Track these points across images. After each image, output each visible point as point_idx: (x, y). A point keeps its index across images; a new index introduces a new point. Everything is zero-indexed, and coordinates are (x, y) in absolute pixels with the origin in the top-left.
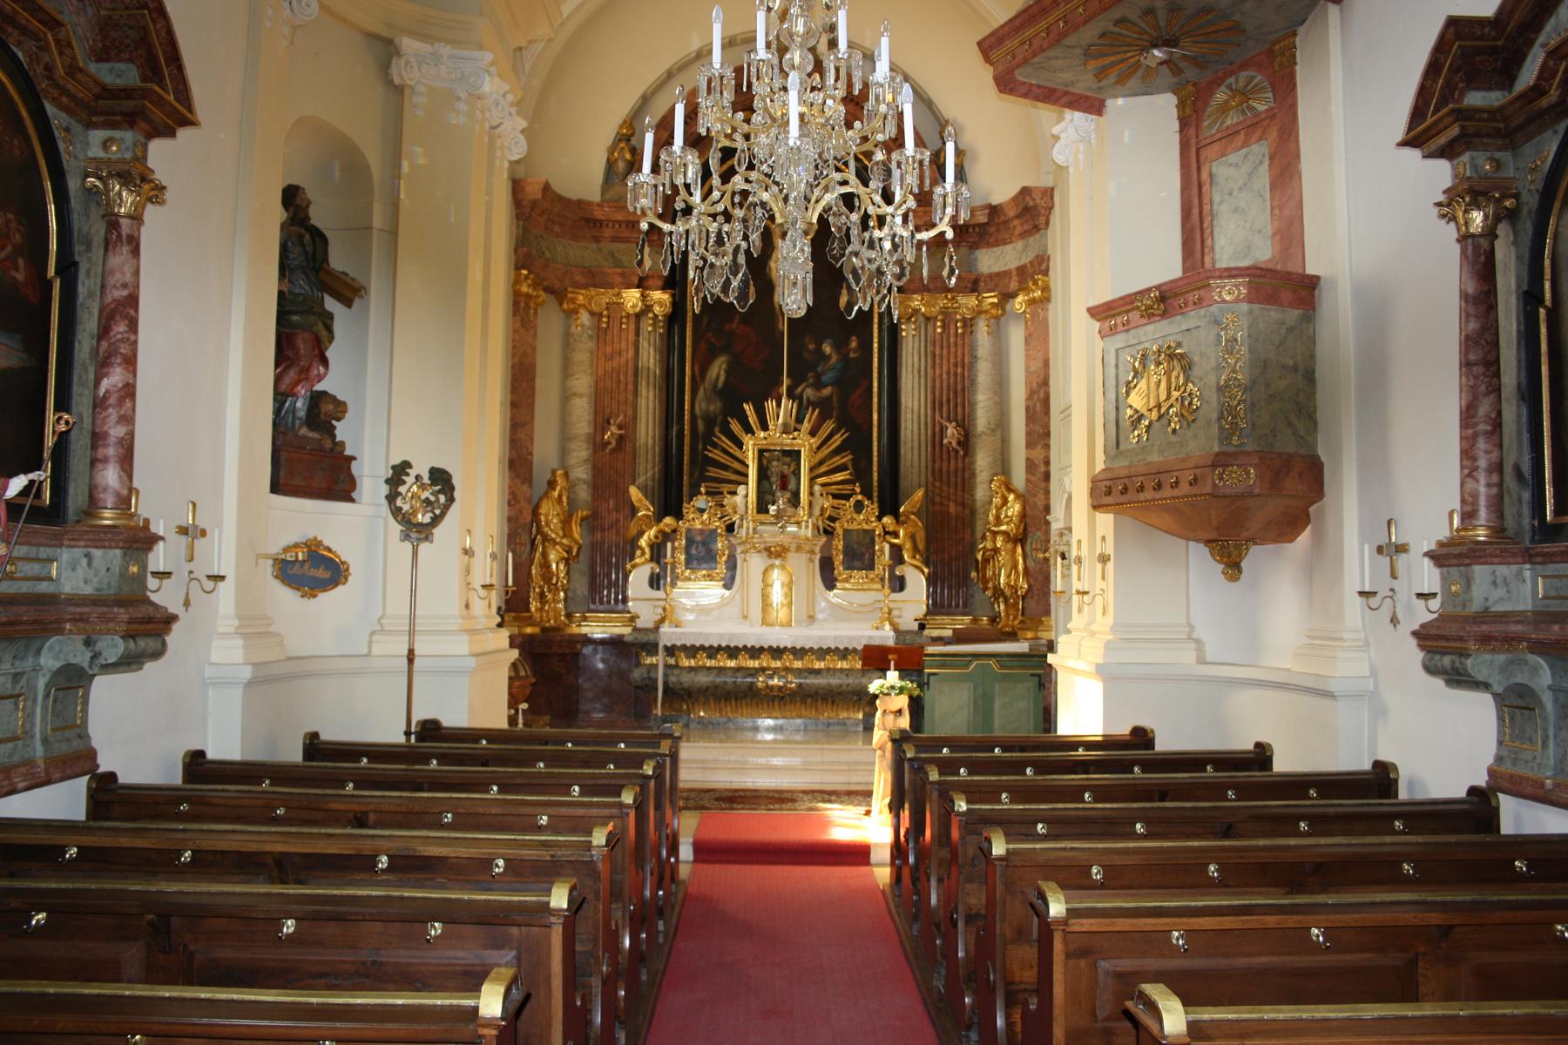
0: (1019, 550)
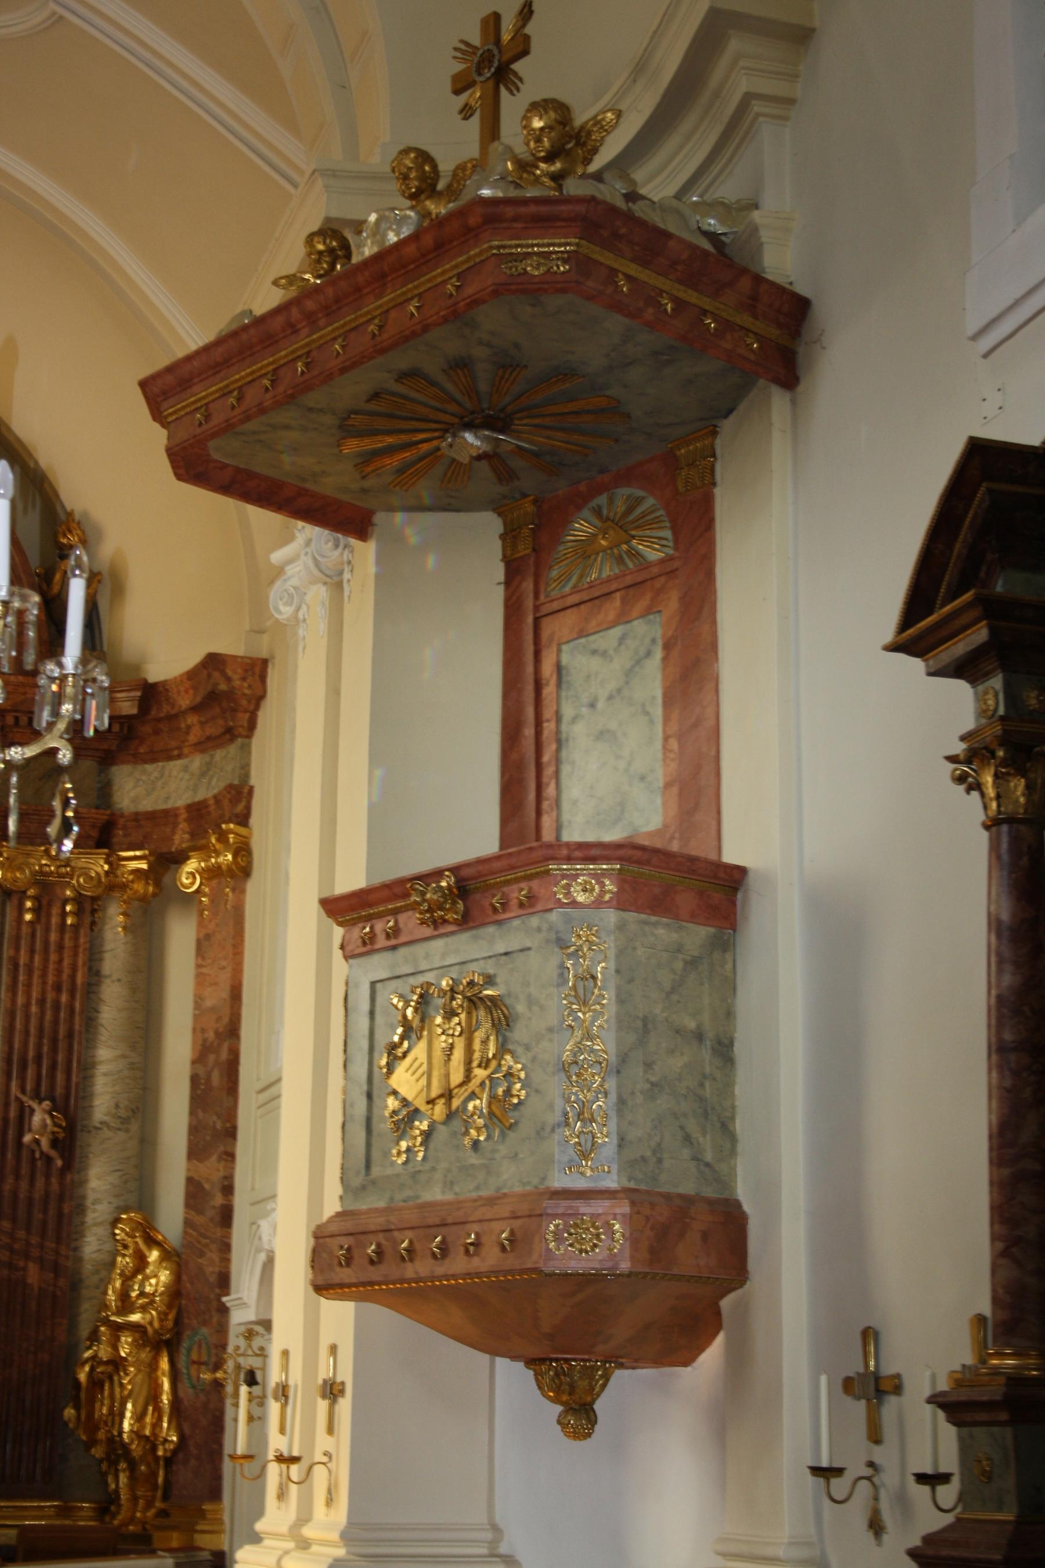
0: (164, 1364)
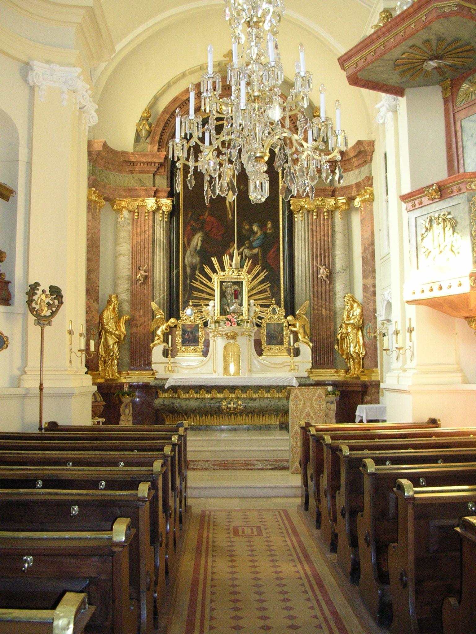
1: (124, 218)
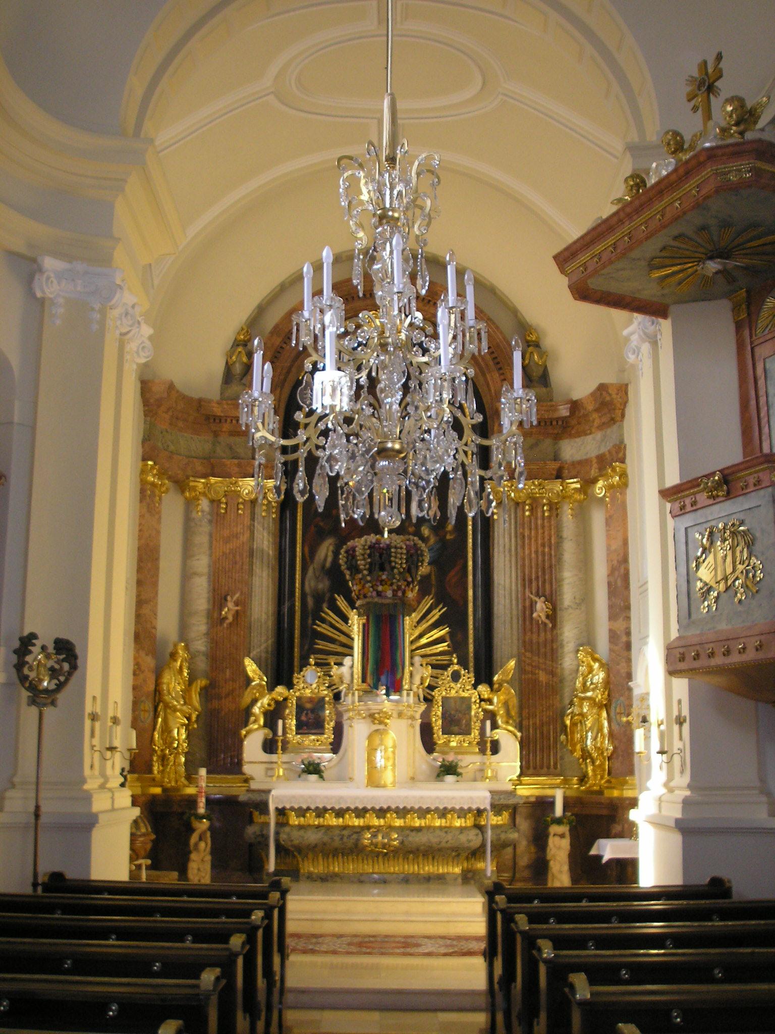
0: (604, 714)
1: (203, 511)
